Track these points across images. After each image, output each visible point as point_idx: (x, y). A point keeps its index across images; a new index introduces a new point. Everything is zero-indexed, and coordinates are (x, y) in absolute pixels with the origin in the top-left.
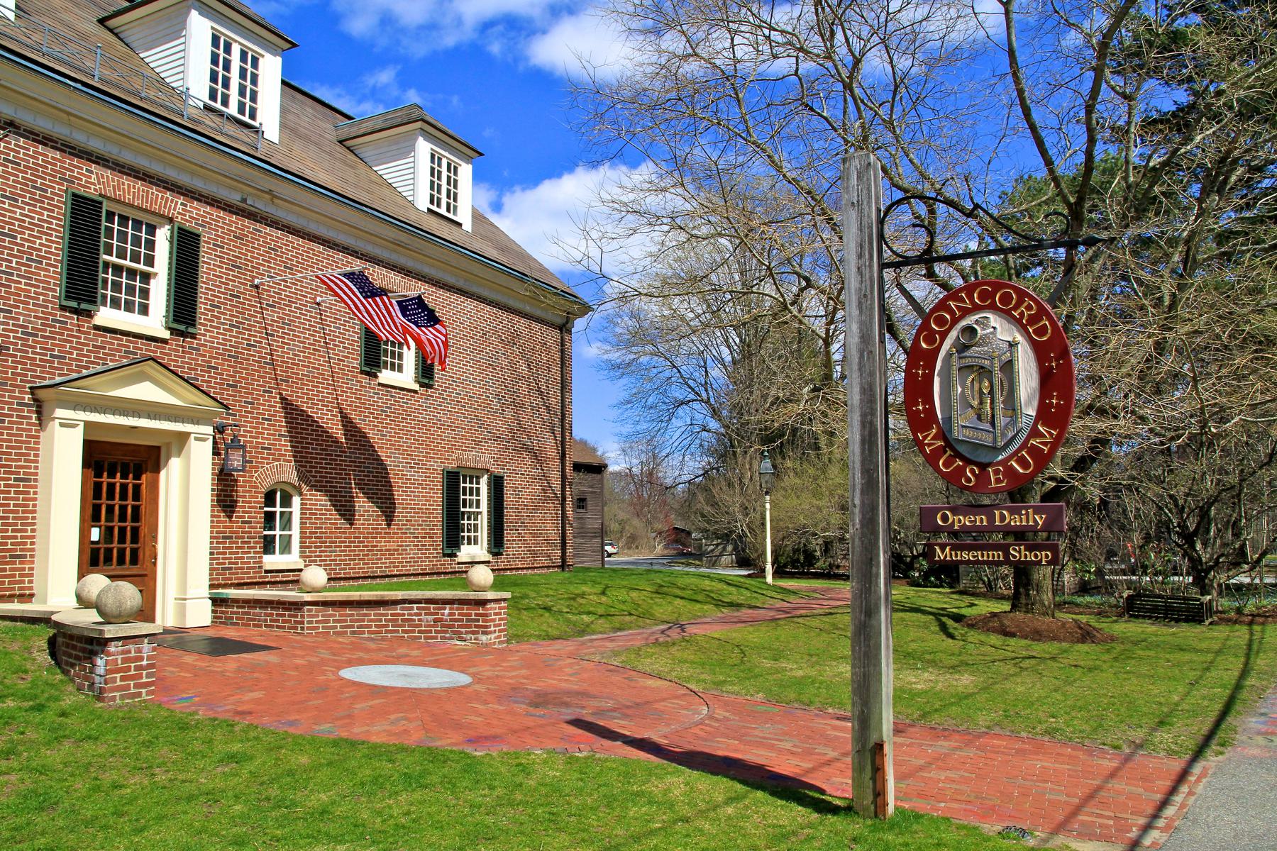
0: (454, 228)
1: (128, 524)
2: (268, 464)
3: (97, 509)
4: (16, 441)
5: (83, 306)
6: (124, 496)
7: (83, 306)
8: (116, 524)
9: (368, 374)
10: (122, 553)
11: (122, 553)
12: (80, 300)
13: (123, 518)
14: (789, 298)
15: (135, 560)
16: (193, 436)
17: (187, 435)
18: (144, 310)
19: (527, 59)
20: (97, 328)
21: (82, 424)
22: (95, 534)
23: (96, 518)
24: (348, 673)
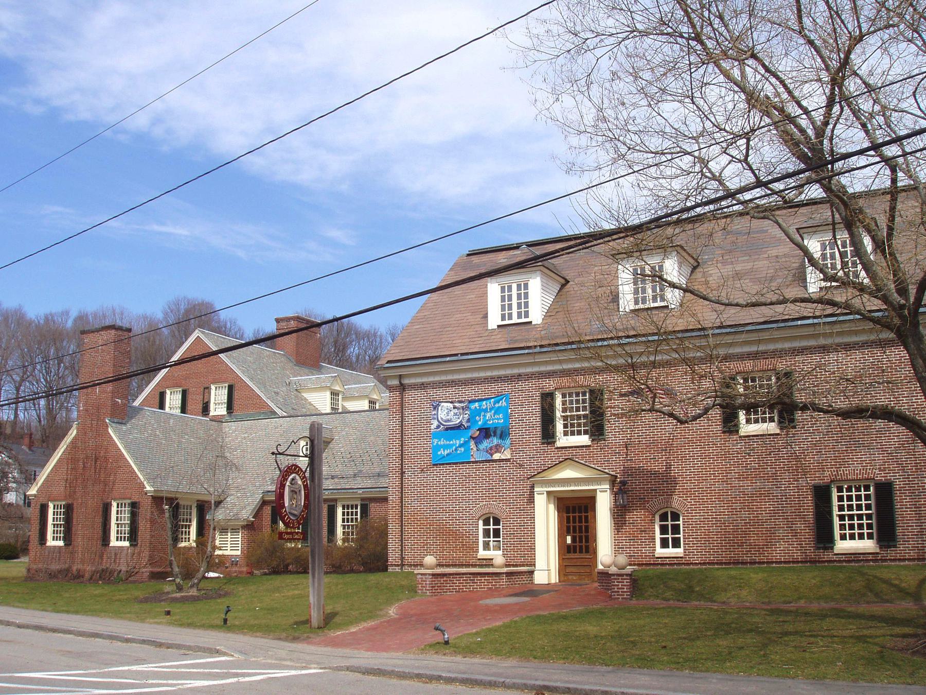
0: (528, 327)
1: (584, 534)
2: (655, 498)
3: (568, 528)
4: (710, 496)
5: (549, 441)
6: (580, 521)
7: (549, 441)
8: (577, 535)
9: (548, 443)
10: (581, 547)
11: (581, 547)
12: (547, 439)
13: (581, 531)
14: (650, 193)
15: (587, 551)
16: (598, 490)
17: (595, 490)
18: (566, 434)
19: (30, 323)
20: (557, 448)
21: (545, 492)
22: (569, 540)
23: (568, 533)
24: (481, 602)
